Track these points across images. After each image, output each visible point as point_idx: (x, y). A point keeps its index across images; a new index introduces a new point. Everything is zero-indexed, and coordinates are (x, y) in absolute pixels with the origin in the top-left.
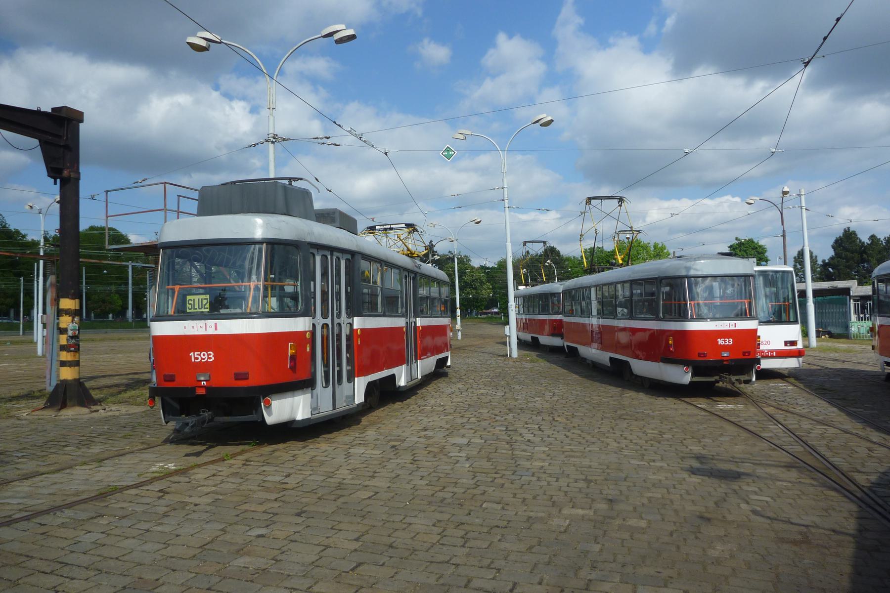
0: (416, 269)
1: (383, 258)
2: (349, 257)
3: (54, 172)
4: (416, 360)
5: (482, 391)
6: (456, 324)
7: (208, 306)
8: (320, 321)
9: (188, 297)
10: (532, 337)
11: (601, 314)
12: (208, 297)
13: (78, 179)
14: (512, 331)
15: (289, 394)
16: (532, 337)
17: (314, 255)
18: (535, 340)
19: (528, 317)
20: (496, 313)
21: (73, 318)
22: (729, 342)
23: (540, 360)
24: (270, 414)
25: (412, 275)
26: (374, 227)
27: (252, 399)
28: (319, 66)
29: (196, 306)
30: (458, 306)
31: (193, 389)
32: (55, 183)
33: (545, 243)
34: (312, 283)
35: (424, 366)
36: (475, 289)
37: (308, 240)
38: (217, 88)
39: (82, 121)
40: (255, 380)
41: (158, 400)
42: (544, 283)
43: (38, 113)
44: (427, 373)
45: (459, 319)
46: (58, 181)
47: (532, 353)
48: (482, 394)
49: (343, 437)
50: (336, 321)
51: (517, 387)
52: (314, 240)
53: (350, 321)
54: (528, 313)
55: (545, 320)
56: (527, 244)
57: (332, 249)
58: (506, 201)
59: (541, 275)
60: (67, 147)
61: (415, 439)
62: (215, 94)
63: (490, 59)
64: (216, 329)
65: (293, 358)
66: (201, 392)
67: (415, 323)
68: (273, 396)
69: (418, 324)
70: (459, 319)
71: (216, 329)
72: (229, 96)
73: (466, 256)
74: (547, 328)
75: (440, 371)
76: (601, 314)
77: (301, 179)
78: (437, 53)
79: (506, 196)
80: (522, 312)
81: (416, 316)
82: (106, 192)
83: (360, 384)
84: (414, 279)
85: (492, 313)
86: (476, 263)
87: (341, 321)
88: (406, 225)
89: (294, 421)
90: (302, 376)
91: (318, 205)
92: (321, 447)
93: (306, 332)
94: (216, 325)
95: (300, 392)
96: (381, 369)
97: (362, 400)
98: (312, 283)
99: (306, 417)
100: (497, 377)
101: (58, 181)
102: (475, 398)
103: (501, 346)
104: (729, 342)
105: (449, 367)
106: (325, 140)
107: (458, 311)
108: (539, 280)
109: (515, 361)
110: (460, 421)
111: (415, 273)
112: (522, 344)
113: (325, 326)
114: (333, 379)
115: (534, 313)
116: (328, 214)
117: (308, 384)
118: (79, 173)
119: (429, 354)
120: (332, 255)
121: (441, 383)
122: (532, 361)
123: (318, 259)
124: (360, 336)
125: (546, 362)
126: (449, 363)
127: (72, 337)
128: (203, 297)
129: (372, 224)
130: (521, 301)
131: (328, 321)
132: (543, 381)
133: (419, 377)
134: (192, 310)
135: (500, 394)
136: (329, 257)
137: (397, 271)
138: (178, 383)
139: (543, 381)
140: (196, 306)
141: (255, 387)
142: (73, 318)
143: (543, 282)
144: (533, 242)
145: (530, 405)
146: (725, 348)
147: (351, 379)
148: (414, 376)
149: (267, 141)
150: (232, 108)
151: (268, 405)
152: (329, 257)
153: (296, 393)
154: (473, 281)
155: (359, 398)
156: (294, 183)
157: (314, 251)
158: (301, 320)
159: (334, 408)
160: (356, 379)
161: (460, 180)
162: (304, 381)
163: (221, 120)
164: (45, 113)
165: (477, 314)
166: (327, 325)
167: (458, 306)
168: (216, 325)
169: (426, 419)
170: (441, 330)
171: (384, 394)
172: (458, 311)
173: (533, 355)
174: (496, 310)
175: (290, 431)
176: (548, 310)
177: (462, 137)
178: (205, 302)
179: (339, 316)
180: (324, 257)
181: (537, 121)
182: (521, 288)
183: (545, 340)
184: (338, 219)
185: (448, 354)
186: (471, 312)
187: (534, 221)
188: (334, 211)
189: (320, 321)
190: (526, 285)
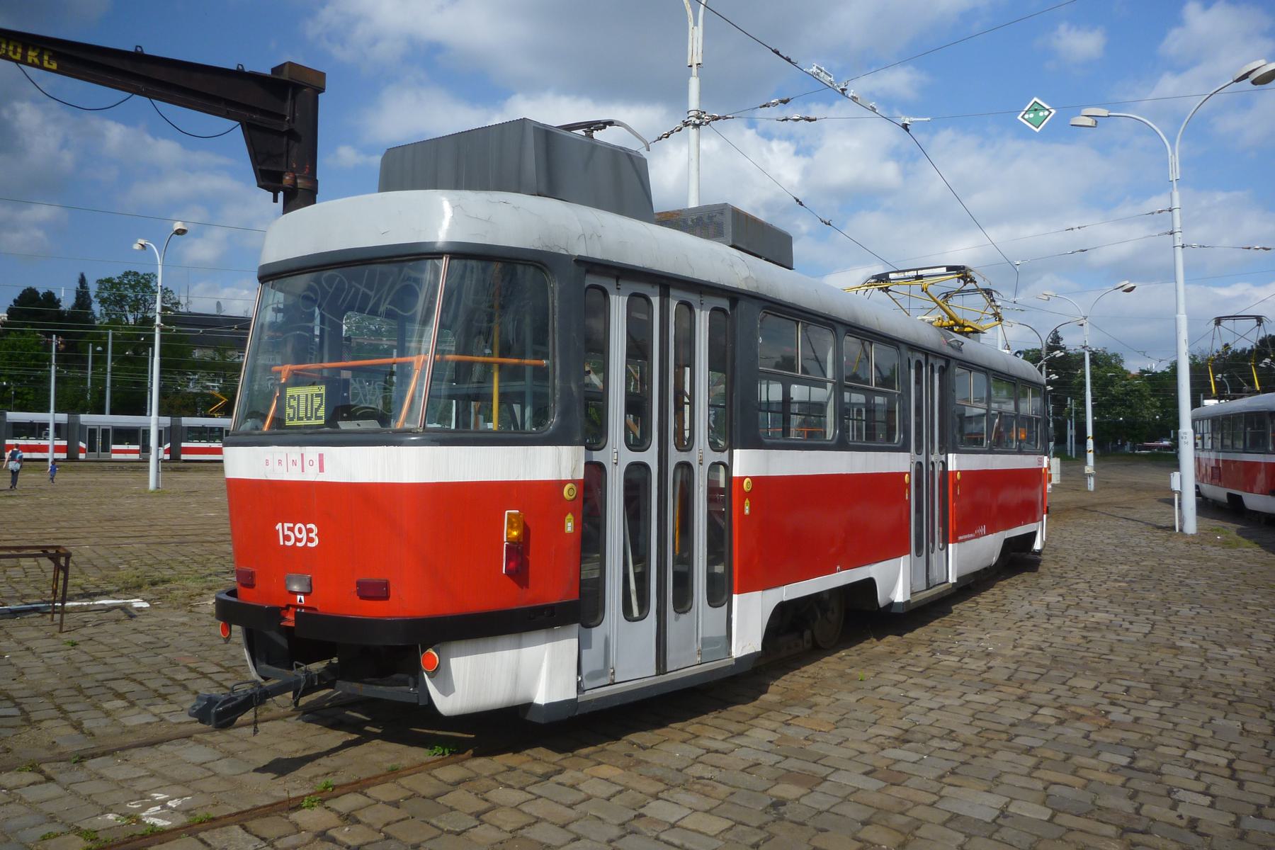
0: (948, 350)
1: (986, 364)
2: (724, 304)
4: (946, 542)
5: (1100, 616)
6: (1086, 463)
7: (322, 412)
10: (1229, 495)
11: (141, 409)
14: (1185, 481)
15: (506, 640)
16: (1229, 495)
17: (605, 294)
18: (1235, 501)
19: (1221, 456)
20: (1166, 448)
23: (1245, 542)
24: (447, 689)
25: (939, 363)
26: (886, 275)
28: (898, 80)
29: (302, 414)
30: (1090, 433)
32: (275, 200)
33: (1259, 319)
34: (688, 370)
35: (985, 547)
36: (1130, 407)
37: (580, 250)
38: (752, 124)
39: (322, 90)
40: (409, 600)
41: (237, 630)
42: (1258, 393)
44: (976, 567)
45: (1090, 456)
46: (281, 195)
47: (1229, 525)
48: (1097, 627)
49: (710, 731)
50: (675, 457)
51: (1185, 611)
52: (597, 253)
53: (724, 457)
54: (1224, 448)
55: (1255, 465)
56: (1224, 323)
57: (666, 282)
58: (1178, 235)
59: (1251, 383)
60: (292, 135)
61: (853, 779)
62: (750, 133)
63: (1174, 42)
64: (321, 469)
65: (518, 551)
67: (945, 464)
68: (454, 646)
70: (1090, 456)
71: (321, 469)
72: (768, 136)
73: (1116, 355)
74: (1261, 478)
75: (1018, 558)
76: (141, 409)
77: (611, 123)
78: (1082, 44)
79: (1177, 224)
80: (1209, 444)
81: (945, 449)
83: (748, 620)
84: (943, 371)
85: (1161, 448)
86: (1133, 366)
87: (692, 457)
88: (950, 268)
89: (528, 706)
90: (550, 588)
92: (597, 773)
93: (562, 483)
94: (321, 456)
95: (542, 634)
96: (830, 570)
98: (688, 370)
99: (558, 697)
100: (1144, 578)
101: (281, 195)
102: (1076, 637)
103: (1165, 508)
107: (1090, 444)
108: (1246, 388)
109: (1190, 541)
110: (1011, 713)
111: (948, 359)
112: (1205, 506)
115: (1233, 449)
116: (710, 218)
117: (577, 611)
118: (316, 181)
119: (983, 529)
120: (664, 296)
121: (1013, 590)
122: (1226, 544)
123: (618, 306)
124: (749, 495)
125: (1257, 548)
126: (1037, 546)
128: (315, 390)
129: (879, 270)
130: (1206, 427)
132: (1248, 598)
133: (952, 579)
134: (295, 423)
135: (1141, 628)
136: (656, 301)
137: (982, 376)
139: (1248, 598)
140: (302, 414)
141: (423, 620)
143: (1254, 392)
144: (1234, 317)
145: (1213, 672)
146: (298, 556)
147: (719, 594)
148: (936, 575)
149: (686, 124)
150: (770, 150)
151: (441, 672)
152: (656, 301)
153: (526, 637)
154: (1127, 394)
156: (597, 135)
157: (608, 284)
158: (548, 451)
160: (735, 597)
161: (1116, 238)
162: (551, 608)
163: (754, 166)
165: (1133, 449)
167: (1090, 433)
168: (321, 456)
169: (926, 700)
170: (1035, 477)
172: (1090, 444)
173: (1230, 529)
174: (1166, 443)
175: (508, 728)
176: (1265, 445)
177: (1089, 122)
178: (317, 401)
179: (685, 444)
180: (638, 303)
181: (1245, 76)
182: (1210, 403)
183: (1255, 501)
184: (728, 229)
186: (1123, 445)
187: (1242, 298)
188: (722, 209)
189: (617, 456)
190: (1220, 397)
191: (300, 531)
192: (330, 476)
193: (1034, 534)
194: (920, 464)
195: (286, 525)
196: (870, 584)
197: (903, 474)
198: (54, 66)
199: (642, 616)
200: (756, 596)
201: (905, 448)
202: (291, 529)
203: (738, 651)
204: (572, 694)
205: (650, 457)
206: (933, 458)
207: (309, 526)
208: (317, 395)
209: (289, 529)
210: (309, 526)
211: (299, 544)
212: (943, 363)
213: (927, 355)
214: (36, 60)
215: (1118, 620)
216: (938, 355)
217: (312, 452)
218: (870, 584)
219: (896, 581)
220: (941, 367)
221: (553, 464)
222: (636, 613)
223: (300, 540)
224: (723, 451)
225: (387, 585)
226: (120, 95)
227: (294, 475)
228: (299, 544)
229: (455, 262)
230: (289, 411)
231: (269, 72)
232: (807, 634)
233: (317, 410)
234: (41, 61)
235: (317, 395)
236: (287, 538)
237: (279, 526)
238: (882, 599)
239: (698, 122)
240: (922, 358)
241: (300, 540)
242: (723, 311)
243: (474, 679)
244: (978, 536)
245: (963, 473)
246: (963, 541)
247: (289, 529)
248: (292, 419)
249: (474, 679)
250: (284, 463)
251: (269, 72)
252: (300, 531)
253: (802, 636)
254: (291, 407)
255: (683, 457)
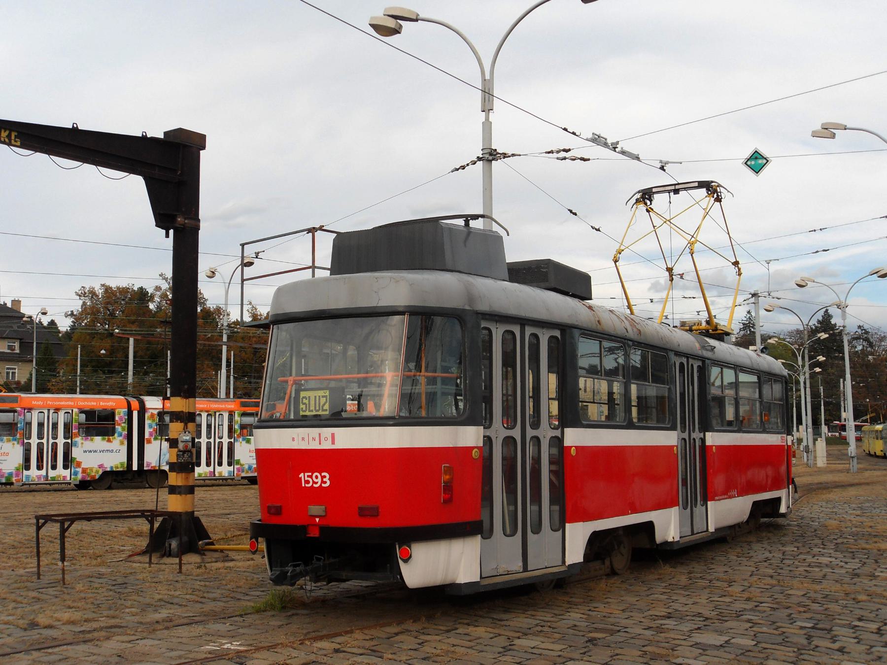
0: (707, 354)
2: (557, 333)
3: (163, 219)
7: (327, 407)
8: (499, 431)
9: (303, 394)
12: (327, 393)
13: (197, 228)
21: (186, 425)
22: (320, 480)
25: (696, 364)
27: (377, 551)
29: (312, 408)
31: (304, 528)
32: (167, 236)
34: (842, 380)
39: (204, 148)
40: (386, 521)
41: (262, 545)
43: (144, 140)
46: (171, 232)
50: (530, 433)
64: (333, 443)
65: (448, 487)
66: (314, 533)
67: (703, 440)
69: (709, 442)
75: (765, 516)
82: (243, 245)
83: (577, 538)
89: (453, 586)
91: (514, 254)
94: (333, 435)
97: (579, 558)
98: (842, 380)
101: (171, 232)
104: (320, 480)
105: (783, 515)
106: (563, 154)
111: (703, 359)
113: (509, 441)
114: (522, 526)
126: (783, 509)
127: (184, 452)
128: (321, 393)
131: (516, 433)
133: (711, 529)
138: (289, 518)
140: (312, 408)
142: (186, 425)
146: (317, 494)
147: (560, 527)
148: (699, 526)
155: (575, 554)
156: (473, 224)
159: (525, 569)
164: (154, 139)
166: (514, 440)
168: (333, 435)
170: (784, 454)
171: (631, 554)
185: (782, 493)
189: (499, 431)
191: (317, 477)
192: (339, 445)
193: (779, 500)
194: (685, 439)
195: (306, 474)
196: (649, 527)
197: (673, 447)
198: (19, 144)
199: (513, 534)
200: (580, 525)
201: (673, 428)
202: (311, 477)
203: (569, 561)
204: (477, 578)
205: (516, 433)
206: (693, 435)
207: (323, 474)
208: (323, 397)
209: (308, 476)
210: (323, 474)
211: (315, 485)
212: (700, 363)
213: (688, 358)
214: (7, 140)
215: (838, 562)
216: (696, 357)
217: (327, 432)
218: (649, 527)
219: (669, 525)
220: (699, 366)
221: (469, 437)
222: (508, 532)
223: (317, 483)
224: (557, 429)
225: (378, 508)
226: (77, 163)
227: (314, 446)
228: (315, 485)
229: (413, 317)
230: (302, 406)
231: (162, 136)
232: (607, 562)
233: (324, 405)
234: (10, 140)
235: (323, 397)
236: (307, 482)
237: (302, 475)
238: (659, 538)
239: (491, 158)
240: (684, 360)
241: (317, 483)
242: (556, 337)
243: (428, 565)
244: (730, 497)
245: (718, 447)
246: (719, 500)
247: (308, 476)
248: (305, 411)
249: (428, 565)
250: (311, 439)
251: (162, 136)
252: (317, 477)
253: (604, 564)
254: (305, 404)
255: (534, 433)
